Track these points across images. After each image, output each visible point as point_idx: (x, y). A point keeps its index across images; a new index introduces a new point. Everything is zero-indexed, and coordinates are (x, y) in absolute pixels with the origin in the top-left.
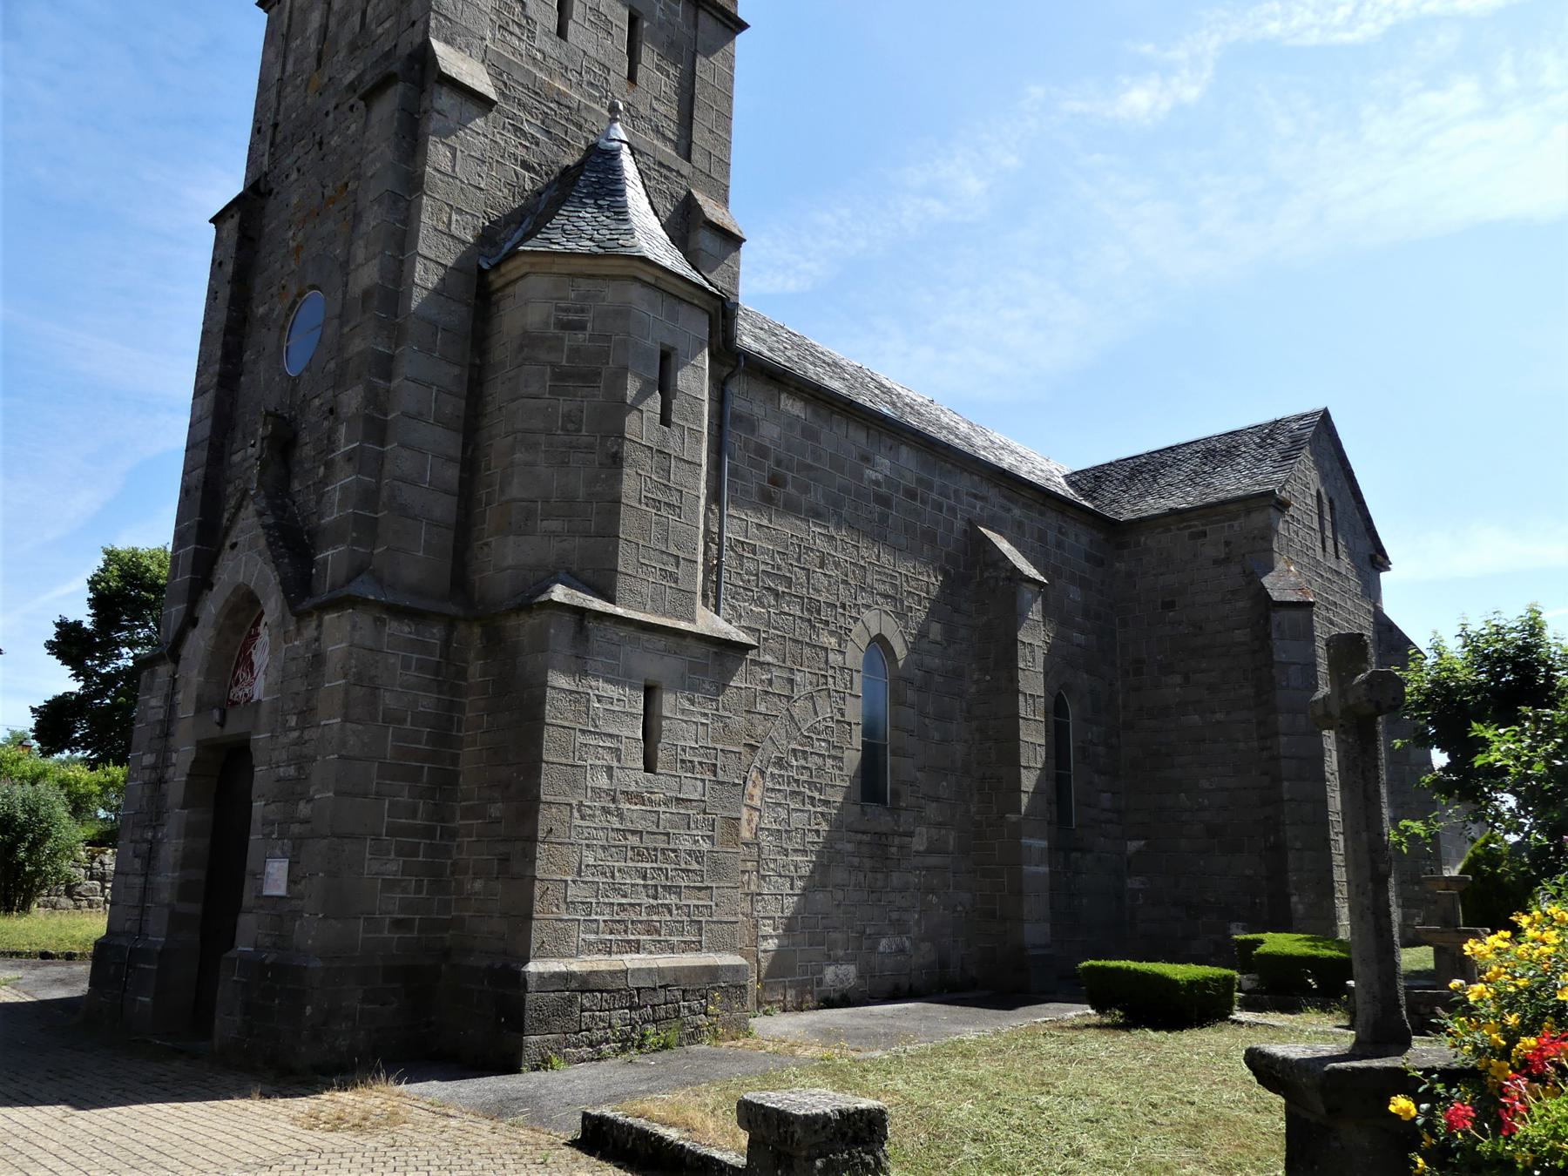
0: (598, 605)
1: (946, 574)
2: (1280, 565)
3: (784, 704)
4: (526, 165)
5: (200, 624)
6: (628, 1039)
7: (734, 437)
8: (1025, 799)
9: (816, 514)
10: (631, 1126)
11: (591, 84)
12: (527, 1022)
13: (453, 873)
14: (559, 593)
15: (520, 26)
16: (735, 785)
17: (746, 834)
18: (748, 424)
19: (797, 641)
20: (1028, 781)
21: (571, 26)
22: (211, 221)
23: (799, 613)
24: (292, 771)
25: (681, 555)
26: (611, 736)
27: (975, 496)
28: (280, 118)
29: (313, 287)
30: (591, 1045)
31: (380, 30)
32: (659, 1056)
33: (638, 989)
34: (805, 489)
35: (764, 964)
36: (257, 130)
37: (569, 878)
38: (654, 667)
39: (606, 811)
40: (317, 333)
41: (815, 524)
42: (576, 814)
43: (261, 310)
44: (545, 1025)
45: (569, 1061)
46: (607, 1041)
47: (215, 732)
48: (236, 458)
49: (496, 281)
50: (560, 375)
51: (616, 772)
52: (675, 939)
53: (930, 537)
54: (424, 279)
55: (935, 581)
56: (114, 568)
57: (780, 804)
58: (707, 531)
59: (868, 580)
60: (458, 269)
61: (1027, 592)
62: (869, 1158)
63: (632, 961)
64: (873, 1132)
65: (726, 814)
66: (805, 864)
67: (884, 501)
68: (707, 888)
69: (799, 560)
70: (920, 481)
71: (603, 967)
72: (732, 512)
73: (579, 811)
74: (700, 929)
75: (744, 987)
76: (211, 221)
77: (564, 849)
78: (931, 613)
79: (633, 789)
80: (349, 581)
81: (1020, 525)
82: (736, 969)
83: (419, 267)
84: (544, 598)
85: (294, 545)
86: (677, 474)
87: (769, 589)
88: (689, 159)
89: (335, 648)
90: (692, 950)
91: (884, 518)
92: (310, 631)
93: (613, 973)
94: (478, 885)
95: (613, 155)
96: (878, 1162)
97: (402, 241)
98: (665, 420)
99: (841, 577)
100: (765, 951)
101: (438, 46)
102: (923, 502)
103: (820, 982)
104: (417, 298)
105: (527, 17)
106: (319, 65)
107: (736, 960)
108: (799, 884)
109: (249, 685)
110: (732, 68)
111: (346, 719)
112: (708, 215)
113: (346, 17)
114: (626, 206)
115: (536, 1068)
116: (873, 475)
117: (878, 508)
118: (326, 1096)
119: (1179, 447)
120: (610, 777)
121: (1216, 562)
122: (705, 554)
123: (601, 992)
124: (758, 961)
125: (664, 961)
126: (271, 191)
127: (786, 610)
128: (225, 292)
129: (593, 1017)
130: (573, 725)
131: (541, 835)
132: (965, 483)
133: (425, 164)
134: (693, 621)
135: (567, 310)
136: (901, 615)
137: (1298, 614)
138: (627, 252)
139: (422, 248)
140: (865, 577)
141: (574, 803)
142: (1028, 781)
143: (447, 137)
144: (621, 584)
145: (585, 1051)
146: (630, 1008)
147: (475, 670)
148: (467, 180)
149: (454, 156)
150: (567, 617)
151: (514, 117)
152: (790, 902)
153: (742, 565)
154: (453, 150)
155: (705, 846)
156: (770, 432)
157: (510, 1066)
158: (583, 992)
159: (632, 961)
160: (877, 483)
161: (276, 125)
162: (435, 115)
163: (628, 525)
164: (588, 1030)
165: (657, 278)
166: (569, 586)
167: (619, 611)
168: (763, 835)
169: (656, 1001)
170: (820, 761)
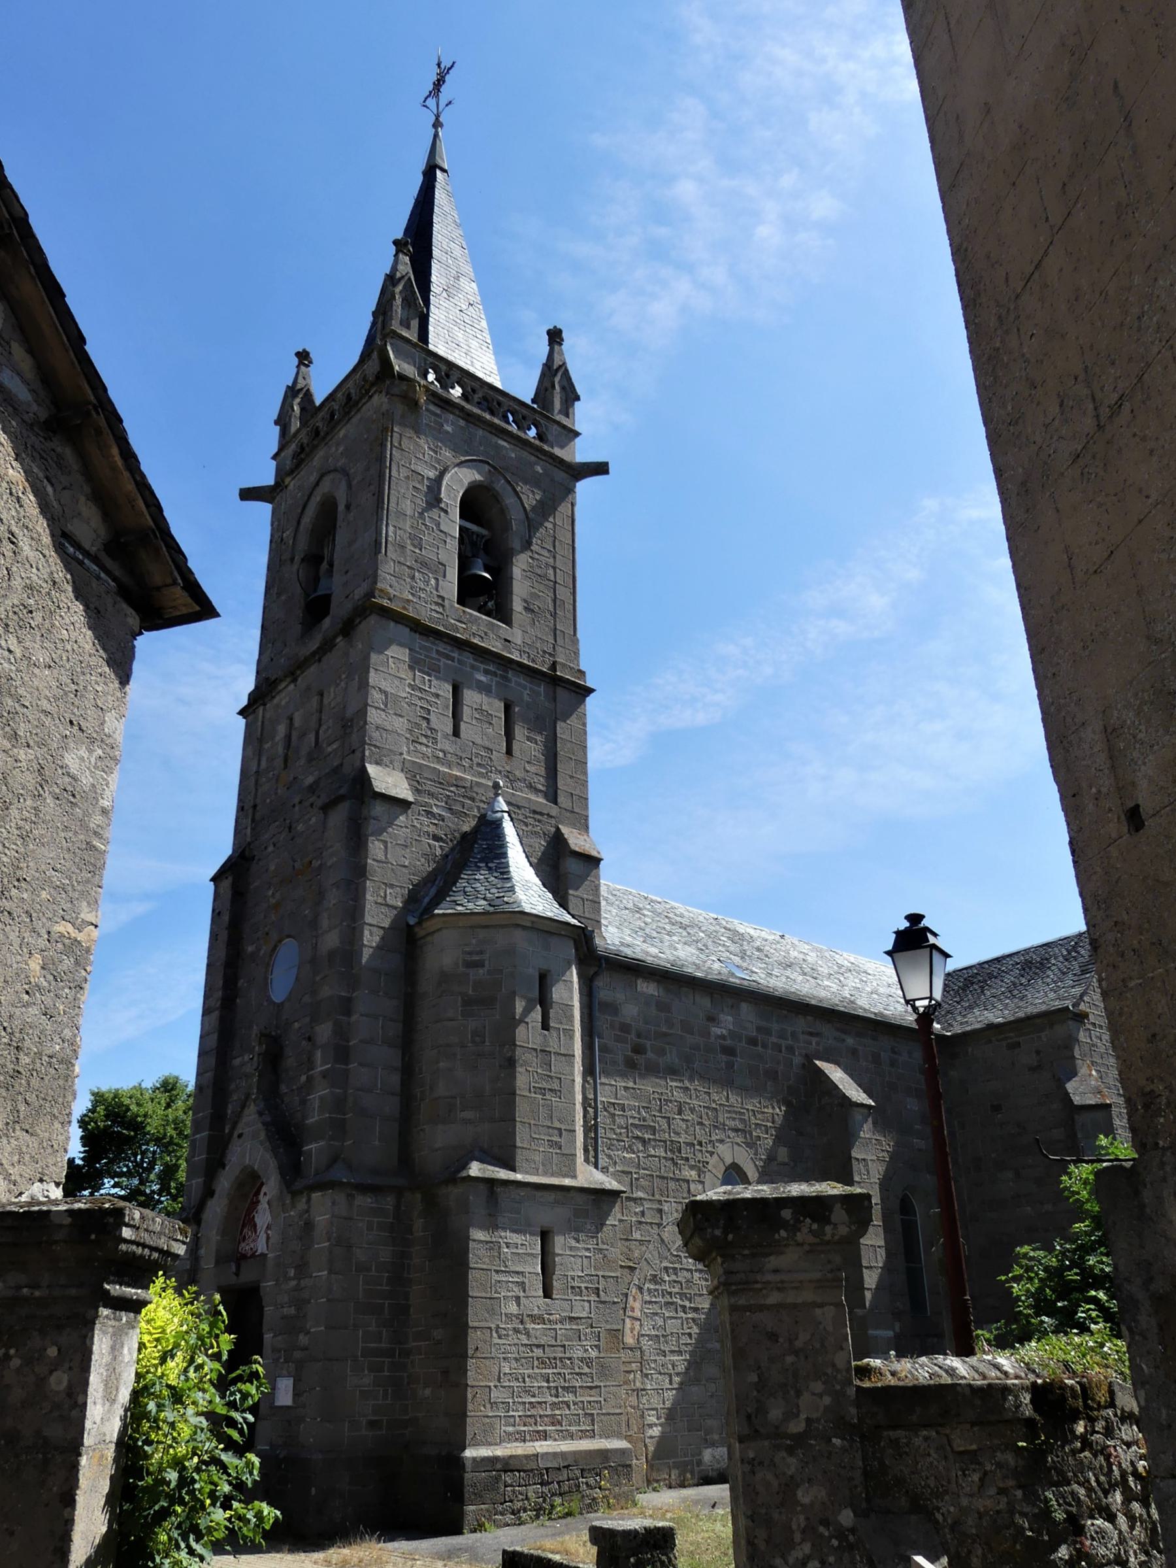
0: (503, 1174)
1: (788, 1104)
2: (1083, 1071)
3: (655, 1230)
4: (436, 838)
5: (216, 1196)
6: (540, 1509)
7: (602, 1021)
8: (868, 1295)
9: (672, 1072)
10: (532, 1555)
11: (479, 765)
12: (466, 1495)
13: (408, 1383)
14: (475, 1169)
15: (426, 736)
16: (614, 1303)
17: (629, 1340)
18: (612, 1008)
19: (663, 1178)
20: (871, 1279)
21: (463, 726)
22: (211, 880)
23: (663, 1154)
24: (292, 1311)
25: (563, 1127)
26: (518, 1273)
27: (811, 1034)
28: (258, 801)
29: (289, 936)
30: (513, 1513)
31: (329, 749)
32: (563, 1521)
33: (547, 1469)
34: (661, 1052)
35: (651, 1449)
36: (241, 808)
37: (492, 1384)
38: (545, 1216)
39: (516, 1331)
40: (295, 970)
41: (672, 1080)
42: (495, 1335)
43: (250, 949)
44: (479, 1498)
45: (498, 1525)
46: (525, 1511)
47: (233, 1280)
48: (237, 1062)
49: (420, 933)
50: (468, 1002)
51: (523, 1300)
52: (573, 1428)
53: (772, 1075)
54: (371, 939)
55: (779, 1111)
56: (101, 1109)
57: (656, 1314)
58: (585, 1098)
59: (721, 1119)
60: (393, 927)
61: (858, 1115)
62: (664, 1558)
63: (542, 1447)
64: (666, 1542)
65: (608, 1327)
66: (680, 1362)
67: (729, 1051)
68: (596, 1387)
69: (660, 1111)
70: (759, 1029)
71: (520, 1452)
72: (604, 1080)
73: (497, 1332)
74: (593, 1420)
75: (630, 1466)
76: (211, 880)
77: (487, 1362)
78: (778, 1140)
79: (536, 1312)
80: (329, 1167)
81: (854, 1052)
82: (623, 1452)
83: (366, 933)
84: (464, 1174)
85: (286, 1137)
86: (557, 1064)
87: (637, 1138)
88: (556, 803)
89: (321, 1219)
90: (587, 1437)
91: (730, 1065)
92: (302, 1205)
93: (527, 1457)
94: (428, 1392)
95: (498, 824)
96: (670, 1560)
97: (354, 913)
98: (545, 1026)
99: (697, 1119)
100: (651, 1437)
101: (371, 769)
102: (764, 1046)
103: (700, 1463)
104: (366, 954)
105: (431, 729)
106: (286, 767)
107: (621, 1444)
108: (677, 1379)
109: (254, 1241)
110: (584, 725)
111: (330, 1272)
112: (573, 847)
113: (303, 735)
114: (506, 853)
115: (475, 1531)
116: (718, 1031)
117: (724, 1058)
118: (331, 1551)
119: (1004, 957)
120: (519, 1305)
121: (1032, 1069)
122: (585, 1117)
123: (519, 1471)
124: (645, 1446)
125: (566, 1446)
126: (253, 858)
127: (653, 1152)
128: (224, 936)
129: (514, 1491)
130: (489, 1267)
131: (470, 1352)
132: (801, 1023)
133: (366, 858)
134: (574, 1177)
135: (470, 953)
136: (751, 1145)
137: (1100, 1115)
138: (507, 908)
139: (368, 919)
140: (717, 1117)
141: (493, 1326)
142: (871, 1279)
143: (380, 834)
144: (520, 1156)
145: (509, 1518)
146: (542, 1484)
147: (418, 1224)
148: (397, 859)
149: (386, 847)
150: (482, 1186)
151: (427, 804)
152: (670, 1395)
153: (614, 1122)
154: (385, 843)
155: (594, 1354)
156: (630, 1011)
157: (457, 1531)
158: (505, 1471)
159: (542, 1447)
160: (723, 1037)
161: (255, 806)
162: (372, 821)
163: (522, 1110)
164: (511, 1501)
165: (533, 922)
166: (482, 1161)
167: (519, 1177)
168: (644, 1341)
169: (561, 1478)
170: (688, 1275)
